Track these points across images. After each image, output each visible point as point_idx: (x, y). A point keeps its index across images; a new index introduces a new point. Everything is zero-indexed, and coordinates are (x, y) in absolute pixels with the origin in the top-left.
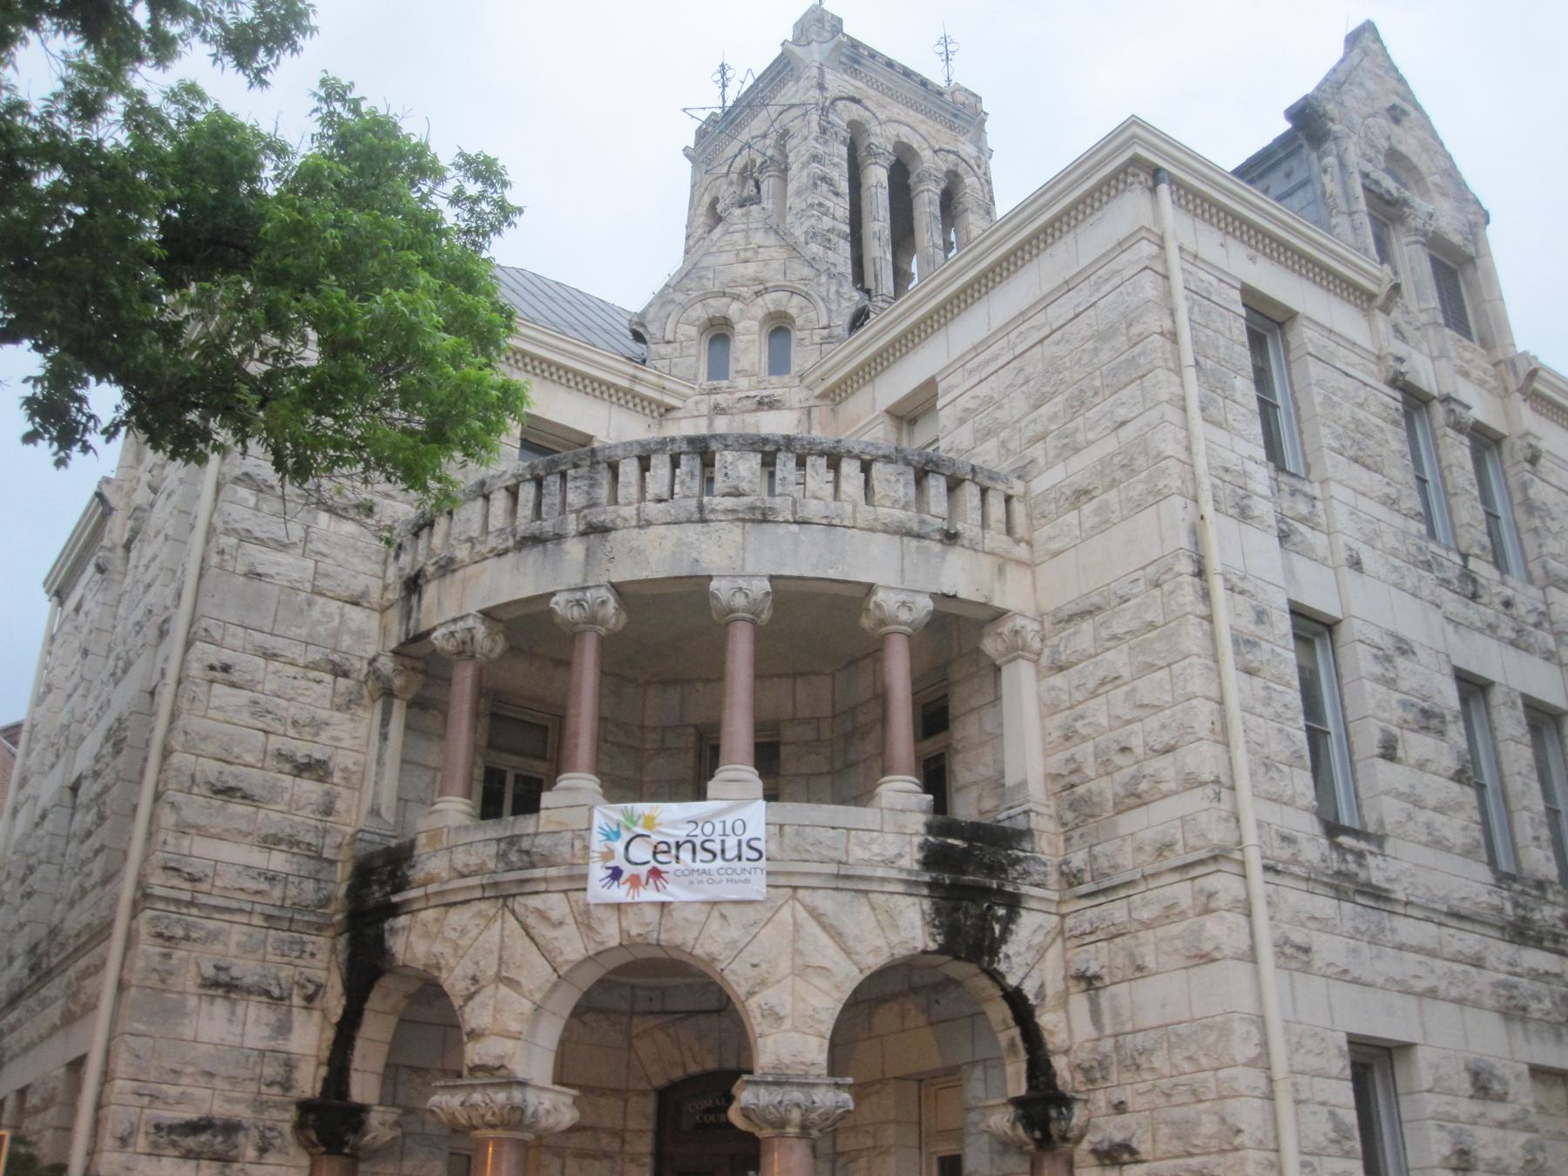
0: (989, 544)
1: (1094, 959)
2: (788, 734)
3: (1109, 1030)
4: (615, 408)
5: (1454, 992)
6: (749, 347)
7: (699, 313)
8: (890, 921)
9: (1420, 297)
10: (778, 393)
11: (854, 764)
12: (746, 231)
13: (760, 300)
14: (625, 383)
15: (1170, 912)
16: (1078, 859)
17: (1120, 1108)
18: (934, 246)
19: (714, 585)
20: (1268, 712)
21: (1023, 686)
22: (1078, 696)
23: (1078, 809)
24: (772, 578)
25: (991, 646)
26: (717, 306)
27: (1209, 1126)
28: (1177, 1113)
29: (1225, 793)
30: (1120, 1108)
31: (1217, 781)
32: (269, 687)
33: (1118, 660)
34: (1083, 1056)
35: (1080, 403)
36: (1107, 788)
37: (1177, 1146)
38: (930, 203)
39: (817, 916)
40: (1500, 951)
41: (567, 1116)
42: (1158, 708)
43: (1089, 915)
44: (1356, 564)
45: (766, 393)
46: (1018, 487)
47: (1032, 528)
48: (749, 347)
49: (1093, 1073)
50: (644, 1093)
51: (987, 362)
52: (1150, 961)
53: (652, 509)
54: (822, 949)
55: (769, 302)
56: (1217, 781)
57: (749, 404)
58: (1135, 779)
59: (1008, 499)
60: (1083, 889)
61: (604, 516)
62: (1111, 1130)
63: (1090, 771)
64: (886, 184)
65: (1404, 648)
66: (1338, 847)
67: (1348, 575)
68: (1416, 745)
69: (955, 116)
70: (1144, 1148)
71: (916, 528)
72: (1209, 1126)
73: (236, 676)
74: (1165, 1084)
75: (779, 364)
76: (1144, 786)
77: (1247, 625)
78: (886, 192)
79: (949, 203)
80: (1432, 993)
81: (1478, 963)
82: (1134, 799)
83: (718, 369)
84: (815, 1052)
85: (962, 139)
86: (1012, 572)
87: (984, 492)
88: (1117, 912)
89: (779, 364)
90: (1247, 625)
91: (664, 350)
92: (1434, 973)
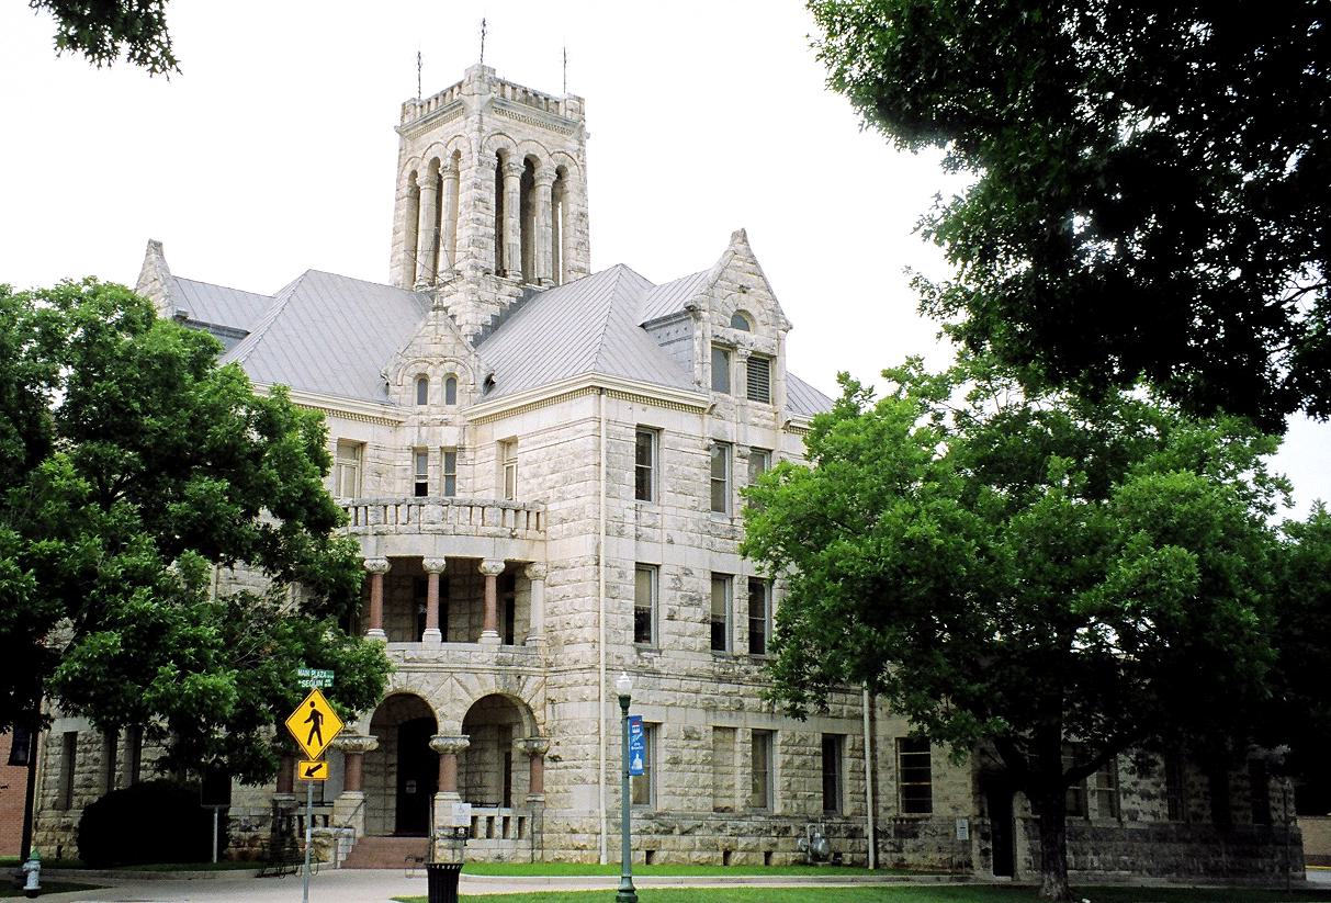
0: (529, 536)
1: (552, 694)
2: (452, 581)
3: (557, 718)
4: (376, 426)
5: (683, 704)
6: (436, 388)
7: (414, 370)
8: (483, 684)
9: (738, 391)
10: (450, 417)
11: (475, 613)
12: (436, 325)
13: (442, 366)
14: (380, 416)
15: (576, 683)
16: (551, 658)
17: (558, 744)
18: (546, 225)
19: (424, 562)
20: (619, 612)
21: (538, 588)
22: (557, 598)
23: (554, 643)
24: (446, 559)
25: (527, 573)
26: (421, 368)
27: (581, 752)
28: (573, 747)
29: (596, 645)
30: (558, 744)
31: (594, 641)
32: (250, 582)
33: (568, 589)
34: (548, 725)
35: (566, 482)
36: (563, 635)
37: (573, 757)
38: (545, 194)
39: (457, 680)
40: (709, 687)
41: (376, 745)
42: (579, 612)
43: (552, 679)
44: (671, 542)
45: (445, 417)
46: (542, 507)
47: (546, 526)
48: (436, 388)
49: (550, 732)
50: (394, 727)
51: (537, 442)
52: (569, 698)
53: (401, 528)
54: (464, 695)
55: (447, 367)
56: (594, 641)
57: (438, 422)
58: (571, 635)
59: (538, 514)
60: (553, 669)
61: (383, 528)
62: (554, 752)
63: (558, 627)
64: (518, 190)
65: (688, 572)
66: (642, 658)
67: (666, 546)
68: (686, 612)
69: (565, 124)
70: (563, 757)
71: (500, 534)
72: (581, 752)
73: (239, 581)
74: (570, 738)
75: (451, 399)
76: (572, 639)
77: (615, 579)
78: (519, 196)
79: (558, 193)
80: (673, 705)
81: (697, 692)
82: (569, 643)
83: (422, 400)
84: (458, 727)
85: (569, 138)
86: (537, 544)
87: (528, 512)
88: (561, 679)
89: (451, 399)
90: (615, 579)
91: (397, 389)
92: (669, 698)
